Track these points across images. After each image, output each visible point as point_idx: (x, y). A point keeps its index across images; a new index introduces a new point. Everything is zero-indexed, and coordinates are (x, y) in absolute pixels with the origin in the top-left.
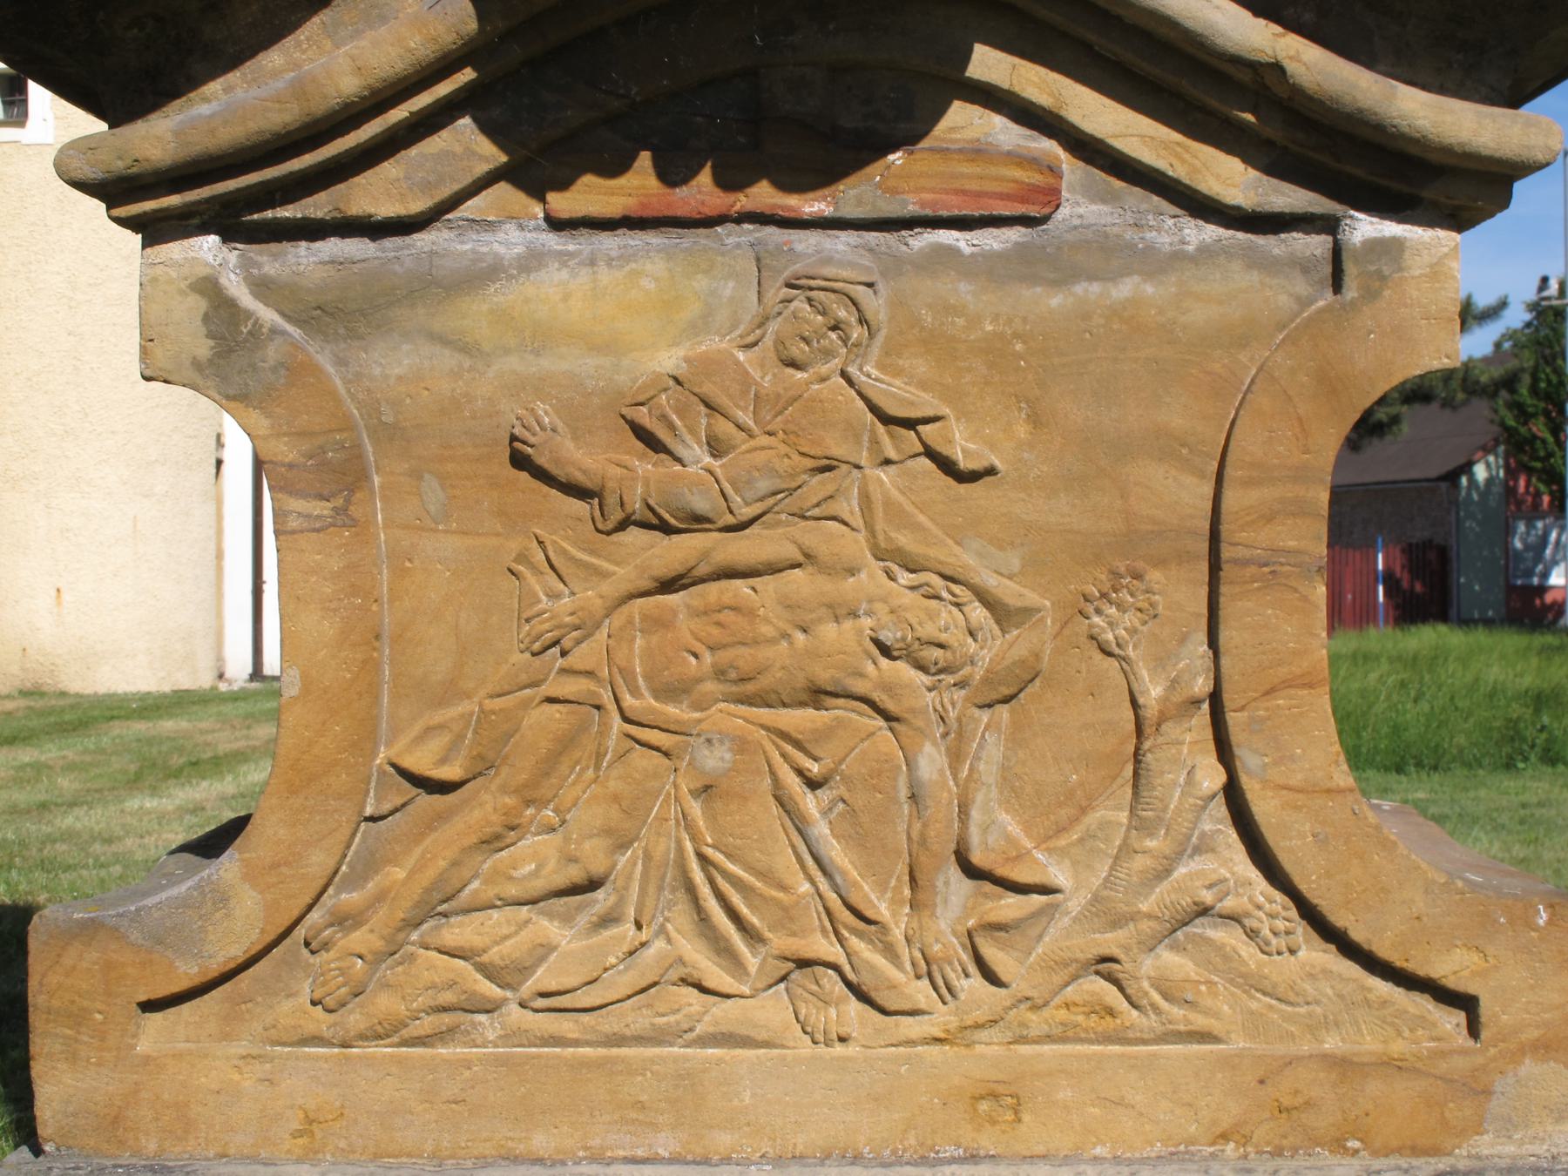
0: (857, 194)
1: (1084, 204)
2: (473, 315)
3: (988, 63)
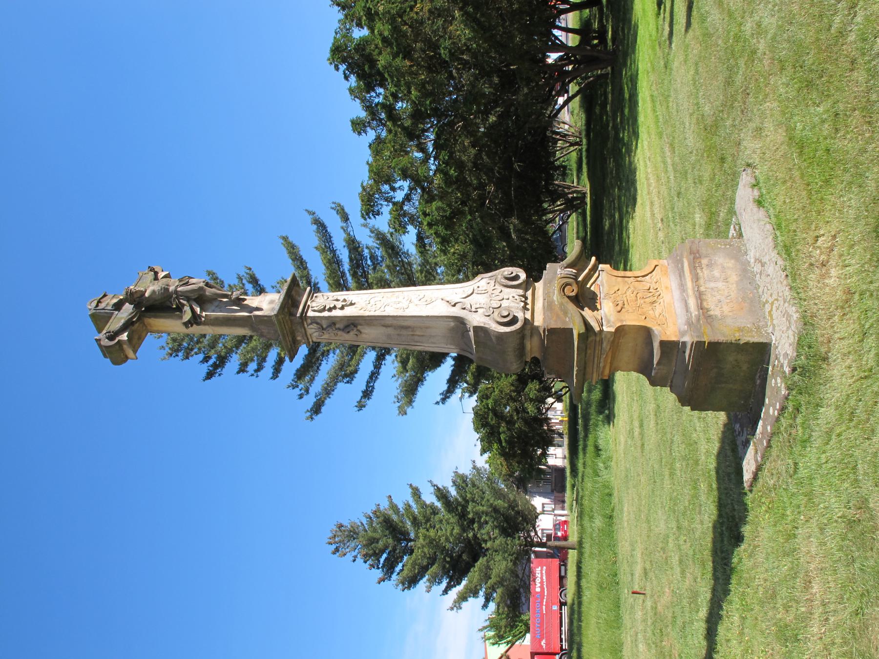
0: (598, 294)
1: (598, 282)
2: (608, 314)
3: (588, 286)
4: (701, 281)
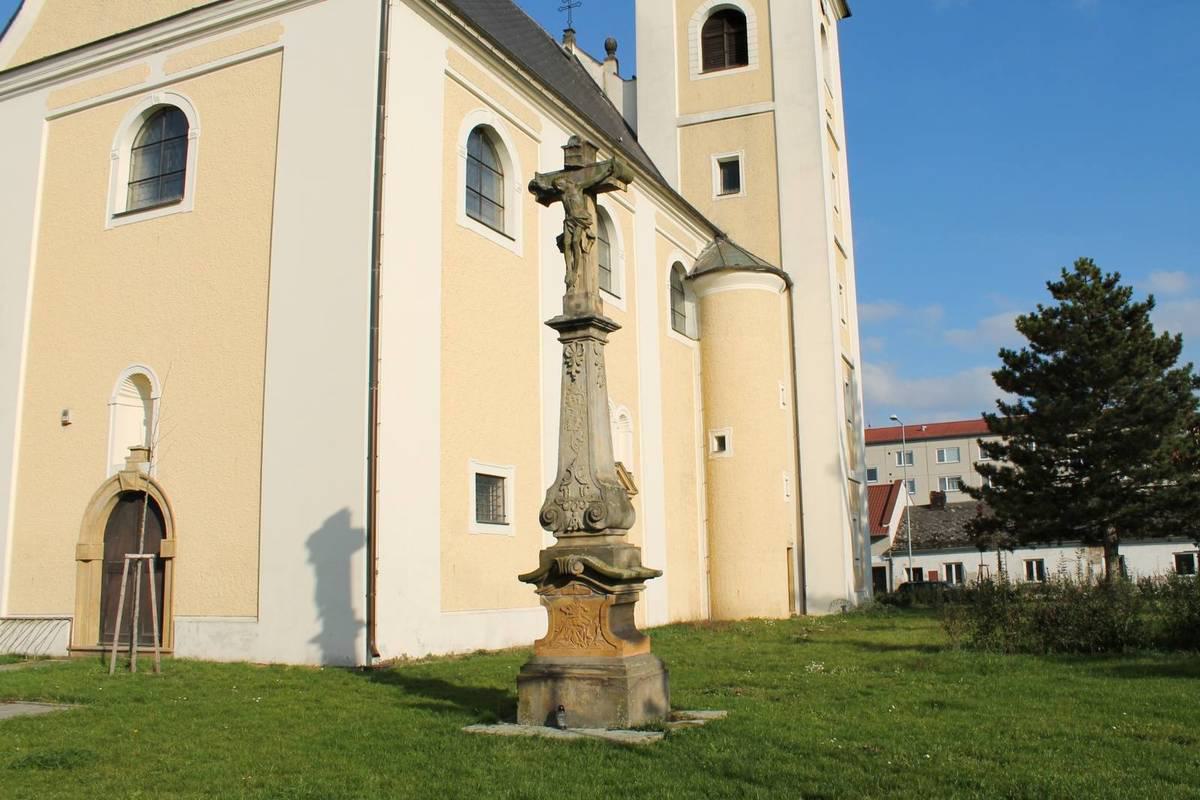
4: (576, 682)
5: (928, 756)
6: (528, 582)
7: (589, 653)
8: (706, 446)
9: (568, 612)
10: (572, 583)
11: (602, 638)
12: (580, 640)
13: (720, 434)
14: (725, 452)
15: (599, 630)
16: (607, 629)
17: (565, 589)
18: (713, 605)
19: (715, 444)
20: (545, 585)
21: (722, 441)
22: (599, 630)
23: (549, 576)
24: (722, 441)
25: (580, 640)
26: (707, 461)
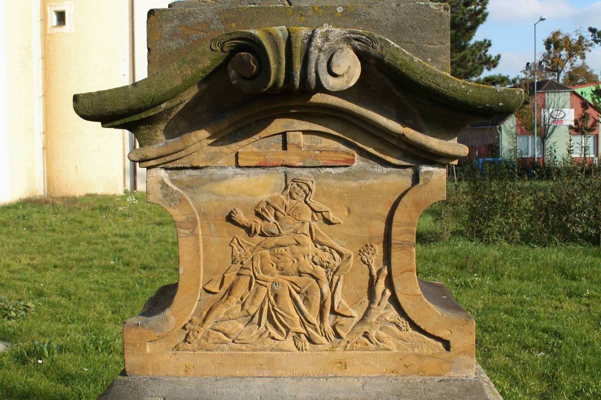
5: (42, 285)
6: (108, 119)
7: (344, 365)
8: (44, 20)
9: (259, 225)
10: (278, 125)
11: (393, 314)
12: (305, 321)
13: (60, 9)
14: (64, 27)
15: (381, 286)
16: (409, 289)
17: (248, 148)
18: (49, 182)
19: (53, 19)
20: (170, 133)
21: (61, 17)
22: (381, 286)
23: (197, 99)
24: (61, 17)
25: (305, 321)
26: (45, 35)
